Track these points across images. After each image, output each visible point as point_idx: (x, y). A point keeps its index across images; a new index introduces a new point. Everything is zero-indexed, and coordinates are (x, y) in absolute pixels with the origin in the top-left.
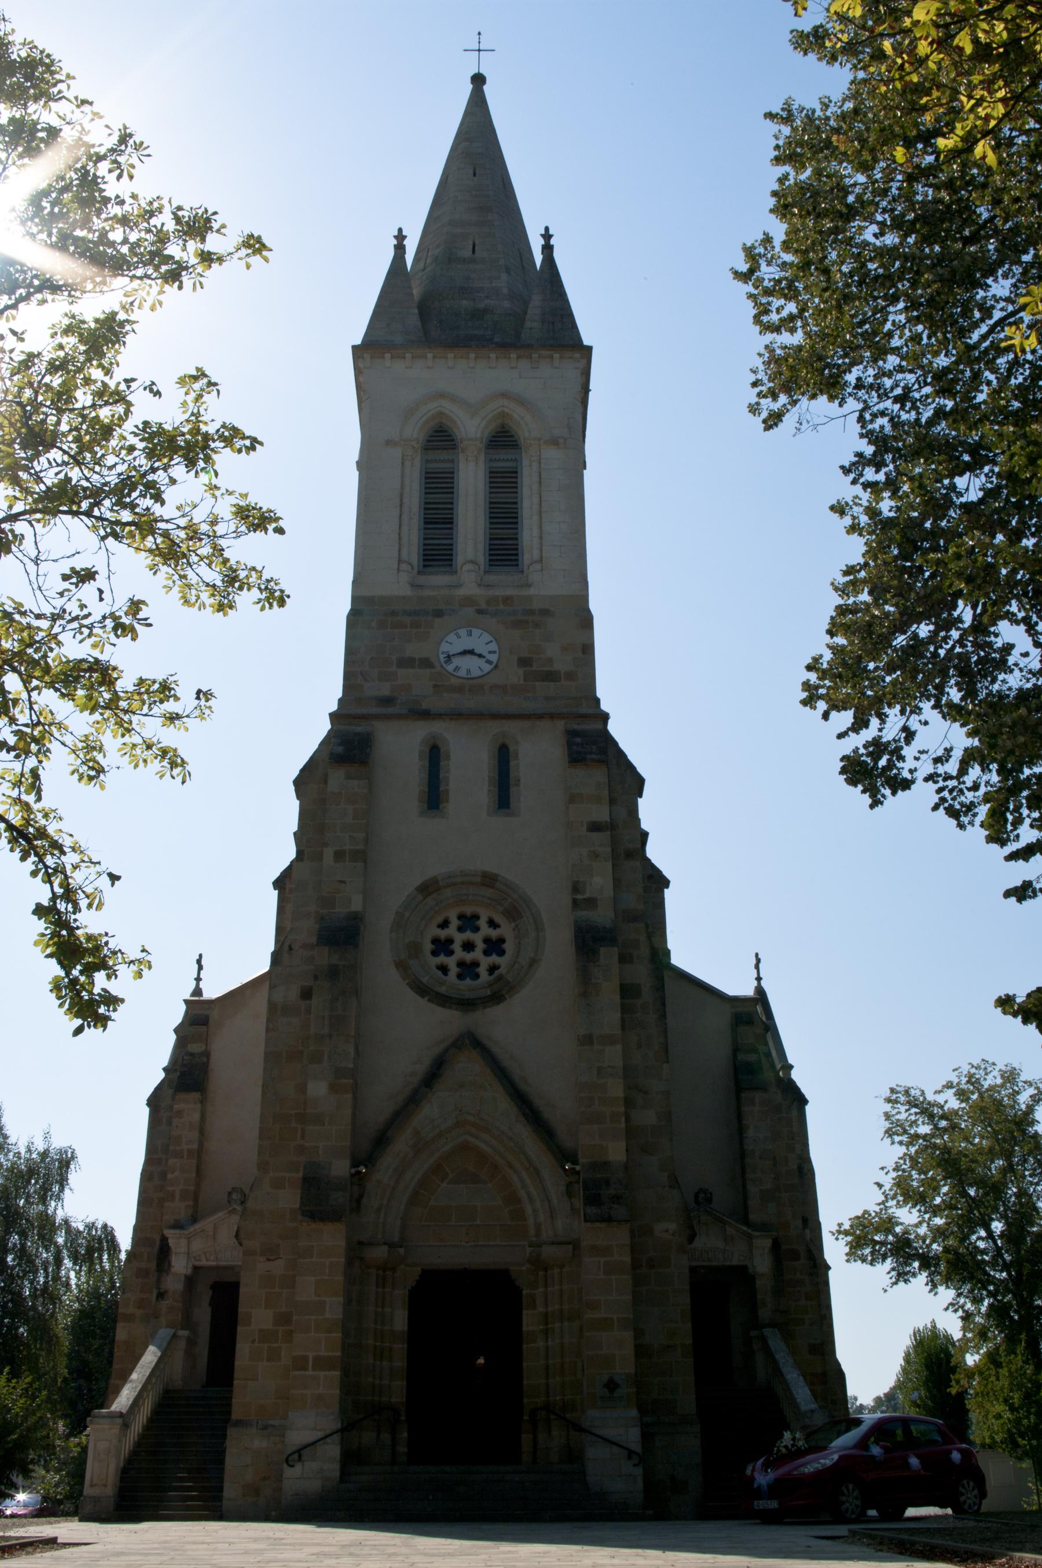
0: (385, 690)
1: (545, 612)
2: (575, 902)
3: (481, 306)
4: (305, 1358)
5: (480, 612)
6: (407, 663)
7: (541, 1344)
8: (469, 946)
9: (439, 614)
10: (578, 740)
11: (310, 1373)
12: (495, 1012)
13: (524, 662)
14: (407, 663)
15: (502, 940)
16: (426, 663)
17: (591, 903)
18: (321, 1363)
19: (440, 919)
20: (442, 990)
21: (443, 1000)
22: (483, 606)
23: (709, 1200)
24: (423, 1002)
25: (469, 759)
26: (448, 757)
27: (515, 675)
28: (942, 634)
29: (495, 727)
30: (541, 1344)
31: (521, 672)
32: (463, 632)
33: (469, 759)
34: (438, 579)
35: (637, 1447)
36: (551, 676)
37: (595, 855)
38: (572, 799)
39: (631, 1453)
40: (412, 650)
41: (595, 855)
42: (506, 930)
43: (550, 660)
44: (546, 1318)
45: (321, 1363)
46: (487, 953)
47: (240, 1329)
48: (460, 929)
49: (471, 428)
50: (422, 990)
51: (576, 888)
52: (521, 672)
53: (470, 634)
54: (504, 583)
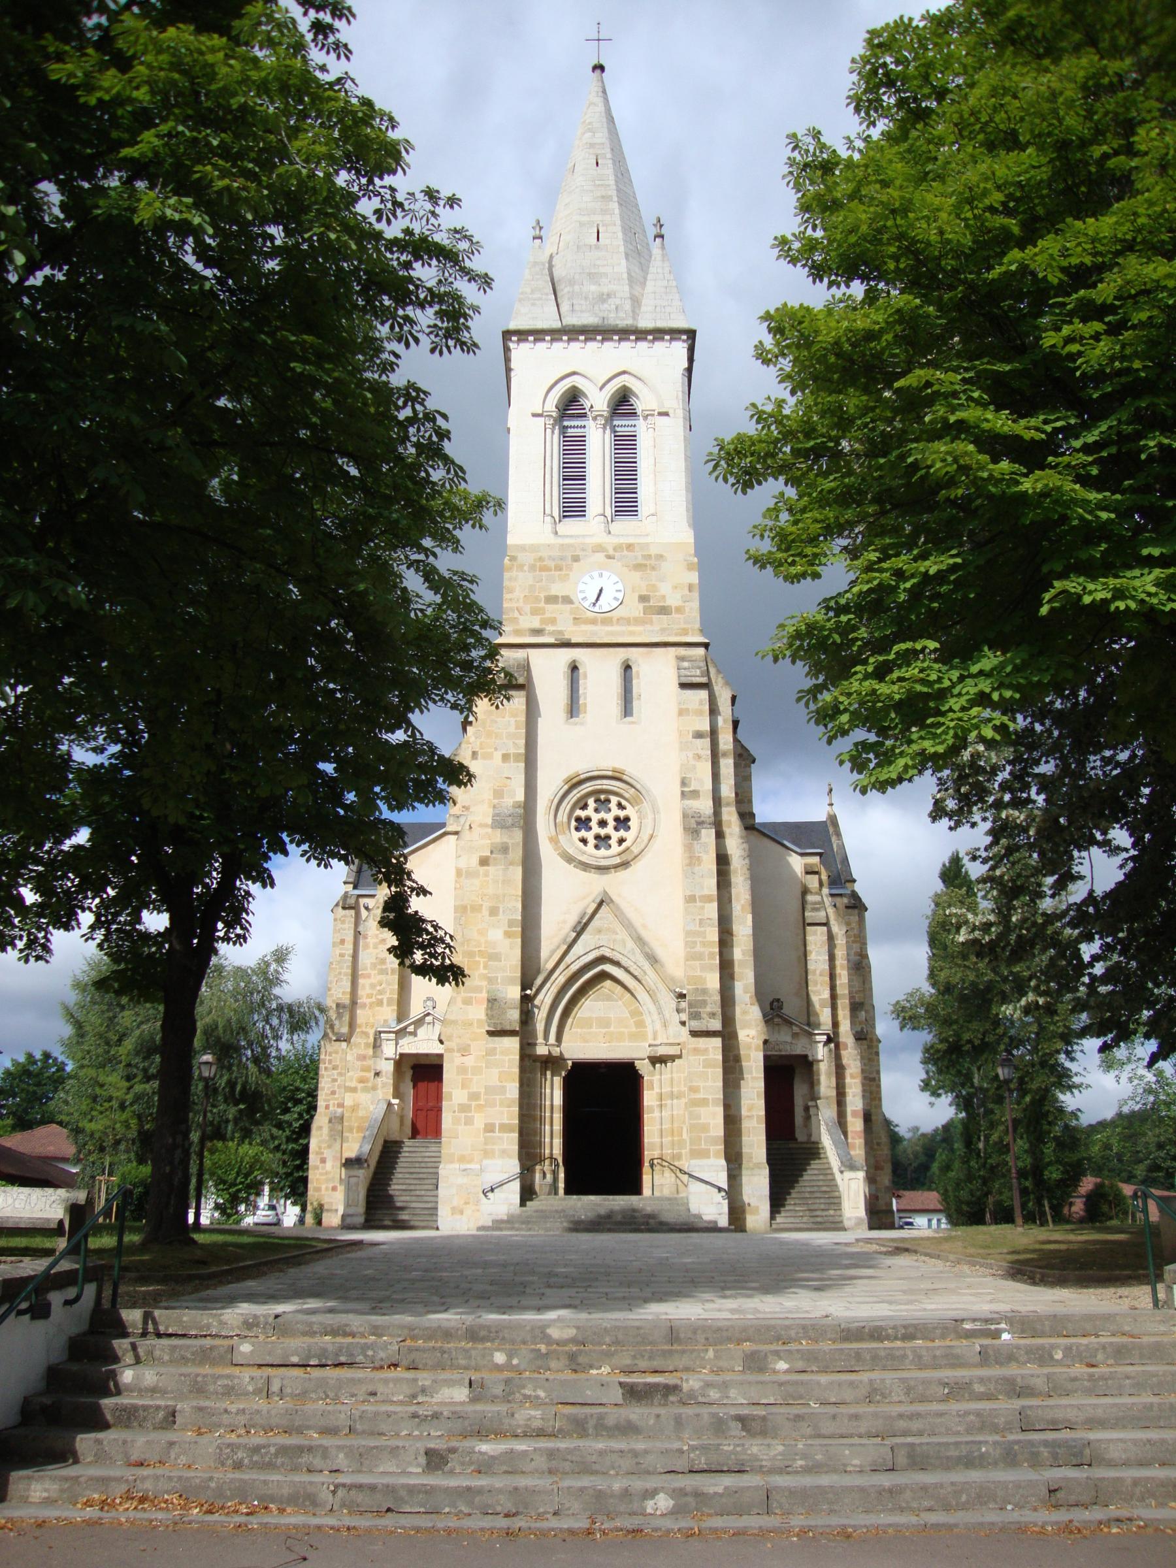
0: (536, 624)
1: (660, 557)
2: (683, 795)
3: (605, 290)
4: (493, 1125)
5: (609, 557)
6: (552, 600)
7: (657, 1114)
8: (603, 823)
9: (576, 559)
10: (686, 664)
11: (497, 1134)
12: (622, 874)
13: (643, 599)
14: (552, 600)
15: (627, 819)
16: (567, 600)
17: (695, 794)
18: (504, 1128)
19: (624, 845)
20: (584, 859)
21: (585, 866)
22: (611, 552)
23: (781, 1008)
24: (570, 868)
25: (601, 672)
26: (585, 677)
27: (635, 609)
28: (830, 1496)
29: (622, 653)
30: (657, 1114)
31: (641, 606)
32: (595, 574)
33: (601, 672)
34: (571, 527)
35: (725, 1187)
36: (664, 610)
37: (699, 757)
38: (681, 712)
39: (720, 1189)
40: (557, 589)
41: (699, 757)
42: (630, 811)
43: (664, 597)
44: (661, 1097)
45: (504, 1128)
46: (616, 829)
47: (445, 1104)
48: (596, 810)
49: (598, 400)
50: (569, 859)
51: (684, 783)
52: (641, 606)
53: (601, 575)
54: (624, 527)
